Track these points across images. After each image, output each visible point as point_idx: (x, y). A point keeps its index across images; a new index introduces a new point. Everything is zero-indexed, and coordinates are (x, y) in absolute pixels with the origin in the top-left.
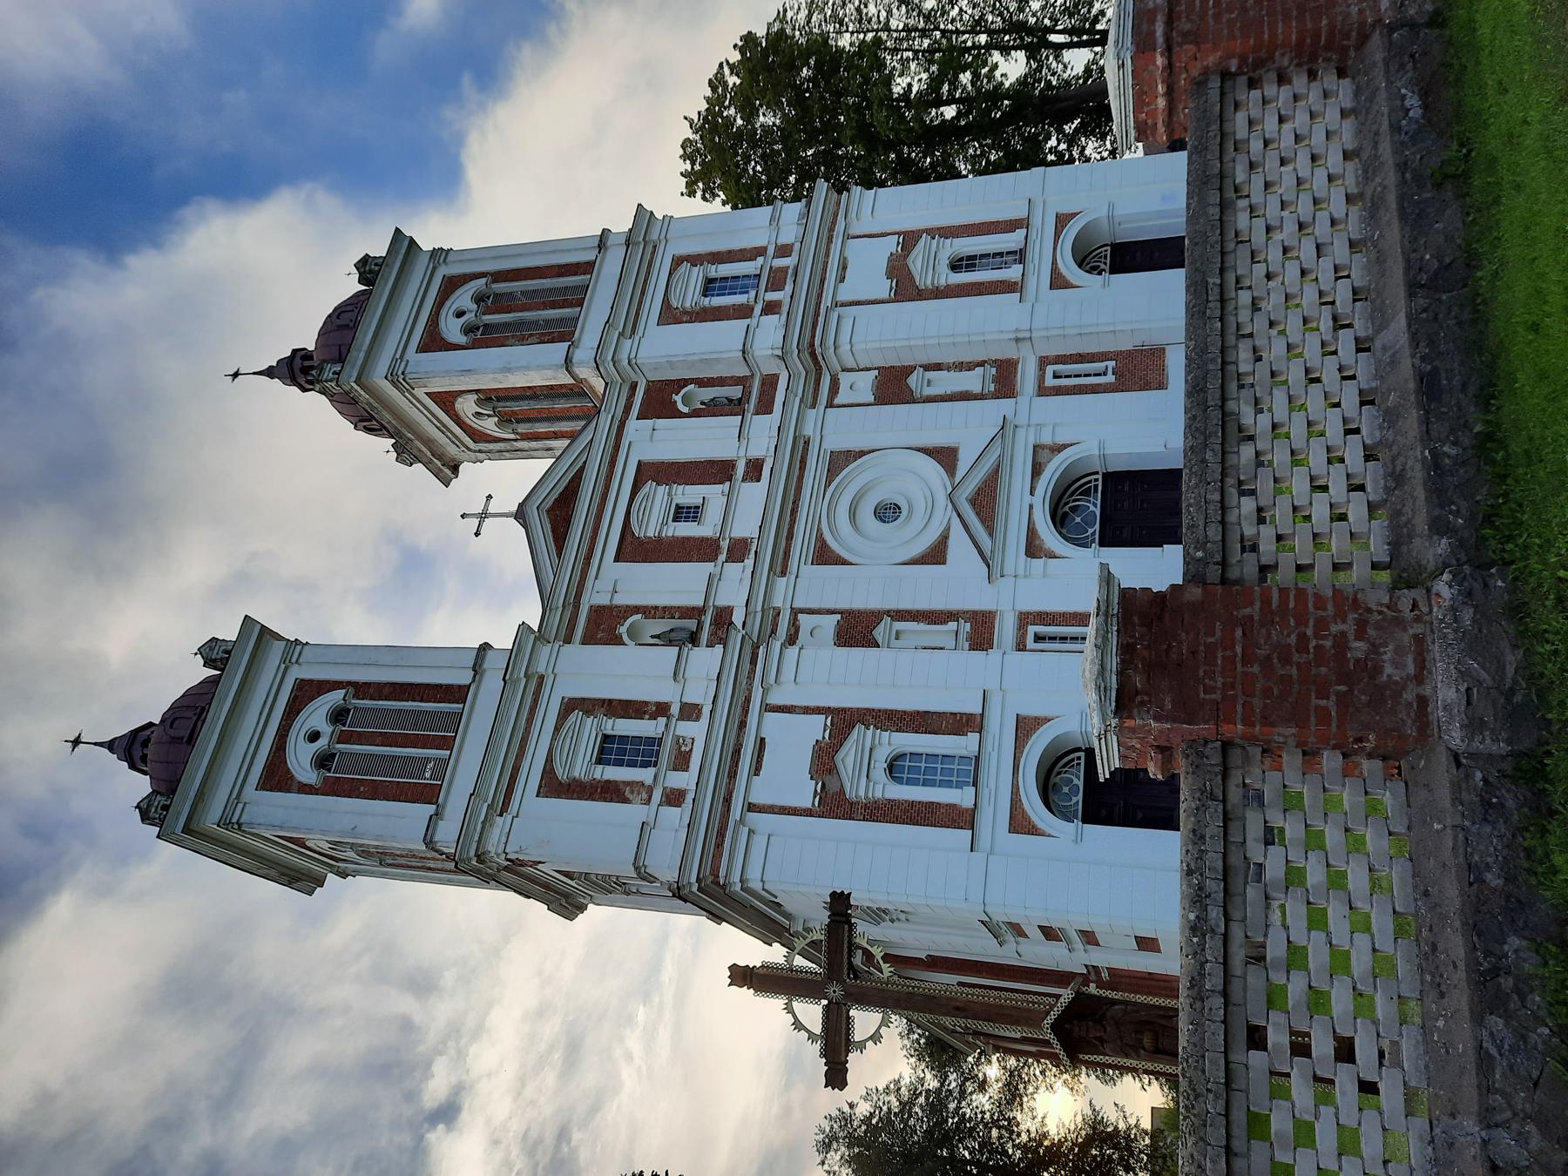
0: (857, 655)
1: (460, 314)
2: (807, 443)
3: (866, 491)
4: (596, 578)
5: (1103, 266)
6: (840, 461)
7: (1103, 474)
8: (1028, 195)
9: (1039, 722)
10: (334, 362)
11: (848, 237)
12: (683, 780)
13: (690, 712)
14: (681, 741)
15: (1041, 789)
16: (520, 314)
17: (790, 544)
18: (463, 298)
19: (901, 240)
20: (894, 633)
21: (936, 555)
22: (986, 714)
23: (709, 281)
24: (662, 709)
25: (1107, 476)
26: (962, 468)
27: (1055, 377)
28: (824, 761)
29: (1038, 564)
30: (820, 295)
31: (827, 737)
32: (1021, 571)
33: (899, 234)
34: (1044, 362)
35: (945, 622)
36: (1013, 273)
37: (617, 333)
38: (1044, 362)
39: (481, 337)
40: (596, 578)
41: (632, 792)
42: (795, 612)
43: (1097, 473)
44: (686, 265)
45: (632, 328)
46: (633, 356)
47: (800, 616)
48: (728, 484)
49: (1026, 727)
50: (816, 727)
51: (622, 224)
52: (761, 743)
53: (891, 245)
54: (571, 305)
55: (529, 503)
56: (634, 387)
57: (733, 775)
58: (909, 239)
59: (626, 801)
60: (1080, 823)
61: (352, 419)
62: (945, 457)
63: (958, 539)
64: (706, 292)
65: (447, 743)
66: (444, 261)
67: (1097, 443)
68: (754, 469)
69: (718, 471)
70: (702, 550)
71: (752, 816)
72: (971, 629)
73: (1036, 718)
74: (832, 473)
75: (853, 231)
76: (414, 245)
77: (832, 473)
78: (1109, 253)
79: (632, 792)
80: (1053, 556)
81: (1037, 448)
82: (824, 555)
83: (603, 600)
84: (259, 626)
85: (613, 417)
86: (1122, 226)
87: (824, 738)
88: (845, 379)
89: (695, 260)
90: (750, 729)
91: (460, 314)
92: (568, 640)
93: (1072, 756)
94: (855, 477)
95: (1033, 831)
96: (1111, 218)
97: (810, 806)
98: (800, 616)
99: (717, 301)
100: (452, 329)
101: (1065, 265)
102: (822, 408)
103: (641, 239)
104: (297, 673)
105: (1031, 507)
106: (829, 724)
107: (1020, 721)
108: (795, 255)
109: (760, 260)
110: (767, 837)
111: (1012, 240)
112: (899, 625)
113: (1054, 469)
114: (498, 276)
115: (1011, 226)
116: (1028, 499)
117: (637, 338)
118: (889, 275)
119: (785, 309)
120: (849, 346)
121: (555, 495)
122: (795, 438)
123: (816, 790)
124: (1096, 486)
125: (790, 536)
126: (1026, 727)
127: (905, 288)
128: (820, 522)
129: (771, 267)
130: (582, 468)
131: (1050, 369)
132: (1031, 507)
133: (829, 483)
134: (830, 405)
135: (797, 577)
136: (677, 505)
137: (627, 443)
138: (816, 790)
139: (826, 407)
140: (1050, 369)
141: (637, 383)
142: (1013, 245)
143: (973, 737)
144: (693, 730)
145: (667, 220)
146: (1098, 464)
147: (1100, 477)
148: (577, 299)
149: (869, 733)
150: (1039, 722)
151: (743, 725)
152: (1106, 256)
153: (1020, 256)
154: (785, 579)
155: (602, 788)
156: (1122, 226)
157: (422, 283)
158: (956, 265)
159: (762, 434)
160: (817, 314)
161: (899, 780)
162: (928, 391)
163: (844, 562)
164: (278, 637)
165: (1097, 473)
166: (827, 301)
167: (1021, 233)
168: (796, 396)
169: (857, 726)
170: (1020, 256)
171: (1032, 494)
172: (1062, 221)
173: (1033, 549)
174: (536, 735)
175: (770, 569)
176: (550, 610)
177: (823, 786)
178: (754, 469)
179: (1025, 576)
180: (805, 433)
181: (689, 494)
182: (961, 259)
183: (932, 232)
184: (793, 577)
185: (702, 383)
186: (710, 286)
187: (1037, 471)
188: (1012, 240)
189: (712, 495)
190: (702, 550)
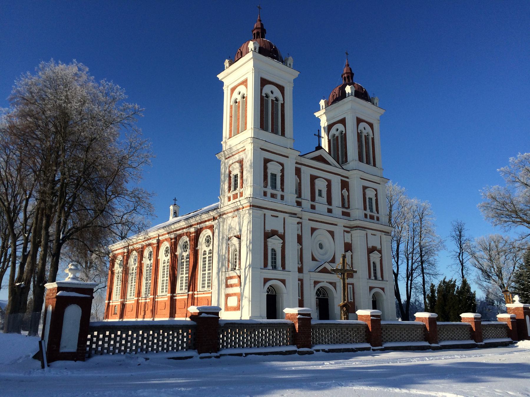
0: (354, 247)
1: (272, 92)
5: (270, 292)
9: (285, 284)
16: (364, 145)
21: (314, 259)
23: (275, 175)
28: (274, 233)
33: (284, 233)
34: (353, 284)
35: (300, 261)
36: (373, 278)
38: (353, 284)
44: (281, 168)
47: (300, 224)
53: (281, 231)
64: (369, 198)
69: (329, 202)
70: (313, 199)
78: (273, 294)
80: (314, 287)
91: (272, 92)
98: (300, 224)
100: (268, 89)
109: (376, 212)
116: (325, 281)
118: (272, 231)
124: (325, 297)
127: (371, 250)
131: (351, 286)
140: (351, 286)
147: (327, 298)
150: (285, 284)
152: (272, 293)
153: (274, 267)
158: (374, 263)
167: (381, 279)
170: (376, 278)
171: (326, 282)
181: (324, 194)
182: (375, 264)
183: (381, 257)
185: (348, 196)
187: (331, 283)
189: (324, 200)
190: (313, 199)
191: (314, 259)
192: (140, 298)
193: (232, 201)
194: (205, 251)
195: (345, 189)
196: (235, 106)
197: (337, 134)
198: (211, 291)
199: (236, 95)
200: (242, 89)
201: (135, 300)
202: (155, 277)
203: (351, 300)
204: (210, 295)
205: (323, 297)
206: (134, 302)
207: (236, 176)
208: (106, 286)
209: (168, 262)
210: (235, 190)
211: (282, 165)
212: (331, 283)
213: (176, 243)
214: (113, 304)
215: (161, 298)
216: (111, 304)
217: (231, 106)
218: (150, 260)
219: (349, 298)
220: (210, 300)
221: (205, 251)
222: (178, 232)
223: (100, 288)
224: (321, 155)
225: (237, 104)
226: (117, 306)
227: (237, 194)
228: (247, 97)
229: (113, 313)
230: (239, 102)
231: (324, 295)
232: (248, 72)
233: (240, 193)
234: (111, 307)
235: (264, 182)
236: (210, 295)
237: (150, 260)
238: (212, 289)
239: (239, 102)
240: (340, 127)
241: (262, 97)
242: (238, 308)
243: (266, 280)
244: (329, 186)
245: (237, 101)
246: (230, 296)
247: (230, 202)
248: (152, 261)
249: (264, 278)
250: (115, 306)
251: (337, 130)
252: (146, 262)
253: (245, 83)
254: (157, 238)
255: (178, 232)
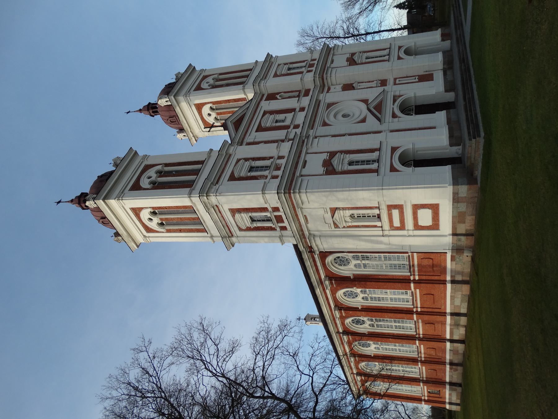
1: (149, 178)
2: (320, 101)
4: (249, 136)
6: (329, 105)
7: (415, 106)
8: (380, 140)
10: (96, 194)
11: (307, 153)
12: (279, 173)
14: (278, 165)
17: (314, 123)
18: (152, 173)
19: (325, 169)
21: (364, 121)
22: (380, 158)
25: (416, 106)
27: (399, 81)
29: (396, 119)
30: (326, 63)
31: (350, 56)
32: (391, 121)
33: (328, 152)
36: (374, 166)
37: (210, 183)
39: (157, 186)
40: (249, 136)
43: (413, 106)
45: (265, 77)
48: (293, 113)
51: (262, 59)
55: (229, 119)
56: (263, 95)
57: (296, 168)
58: (332, 154)
61: (164, 118)
62: (365, 101)
66: (147, 159)
67: (413, 93)
68: (302, 109)
73: (397, 147)
74: (328, 108)
75: (309, 151)
76: (136, 154)
77: (328, 108)
78: (413, 163)
81: (394, 97)
82: (325, 124)
85: (257, 100)
86: (419, 49)
87: (327, 158)
89: (246, 160)
90: (298, 170)
92: (241, 145)
93: (409, 162)
94: (334, 109)
95: (402, 59)
96: (413, 148)
101: (397, 165)
102: (325, 93)
103: (268, 60)
105: (393, 109)
108: (286, 159)
110: (307, 180)
111: (375, 155)
113: (399, 101)
114: (167, 165)
115: (372, 151)
116: (392, 106)
117: (266, 80)
119: (282, 169)
120: (335, 76)
121: (236, 119)
122: (316, 100)
125: (314, 121)
129: (309, 63)
132: (393, 109)
133: (327, 110)
135: (317, 129)
136: (276, 120)
137: (261, 106)
139: (326, 93)
140: (397, 80)
141: (264, 94)
142: (374, 157)
144: (283, 162)
145: (276, 57)
146: (412, 151)
147: (414, 107)
148: (196, 172)
149: (342, 155)
151: (299, 157)
153: (378, 161)
154: (313, 130)
156: (419, 49)
157: (197, 76)
159: (305, 101)
160: (324, 70)
162: (359, 87)
165: (413, 106)
166: (298, 174)
167: (377, 153)
168: (317, 90)
169: (338, 153)
172: (394, 149)
175: (308, 127)
176: (234, 143)
177: (326, 169)
178: (302, 109)
179: (392, 122)
180: (320, 99)
183: (341, 152)
184: (315, 129)
186: (251, 169)
187: (394, 101)
188: (375, 155)
189: (290, 116)
191: (364, 121)
192: (419, 359)
193: (286, 224)
194: (363, 298)
195: (276, 96)
196: (168, 224)
197: (214, 115)
198: (410, 254)
199: (154, 225)
200: (145, 215)
201: (422, 366)
202: (391, 338)
203: (416, 78)
204: (415, 255)
205: (413, 111)
206: (424, 368)
207: (253, 220)
208: (402, 405)
209: (365, 292)
210: (272, 221)
211: (238, 160)
212: (394, 101)
213: (347, 308)
214: (426, 395)
215: (419, 330)
216: (426, 398)
217: (169, 231)
218: (363, 322)
219: (414, 81)
220: (422, 256)
221: (363, 298)
222: (333, 306)
223: (405, 412)
224: (281, 215)
225: (164, 222)
226: (429, 390)
227: (275, 216)
228: (153, 208)
229: (438, 396)
230: (161, 219)
231: (410, 110)
232: (123, 207)
233: (274, 211)
234: (431, 398)
235: (259, 179)
236: (415, 255)
237: (363, 322)
238: (407, 253)
239: (161, 219)
240: (206, 110)
241: (153, 188)
242: (435, 208)
243: (393, 169)
244: (272, 112)
245: (160, 222)
246: (417, 223)
247: (288, 227)
248: (365, 319)
249: (390, 172)
250: (429, 392)
251: (209, 115)
252: (372, 348)
253: (137, 211)
254: (341, 334)
255: (333, 306)
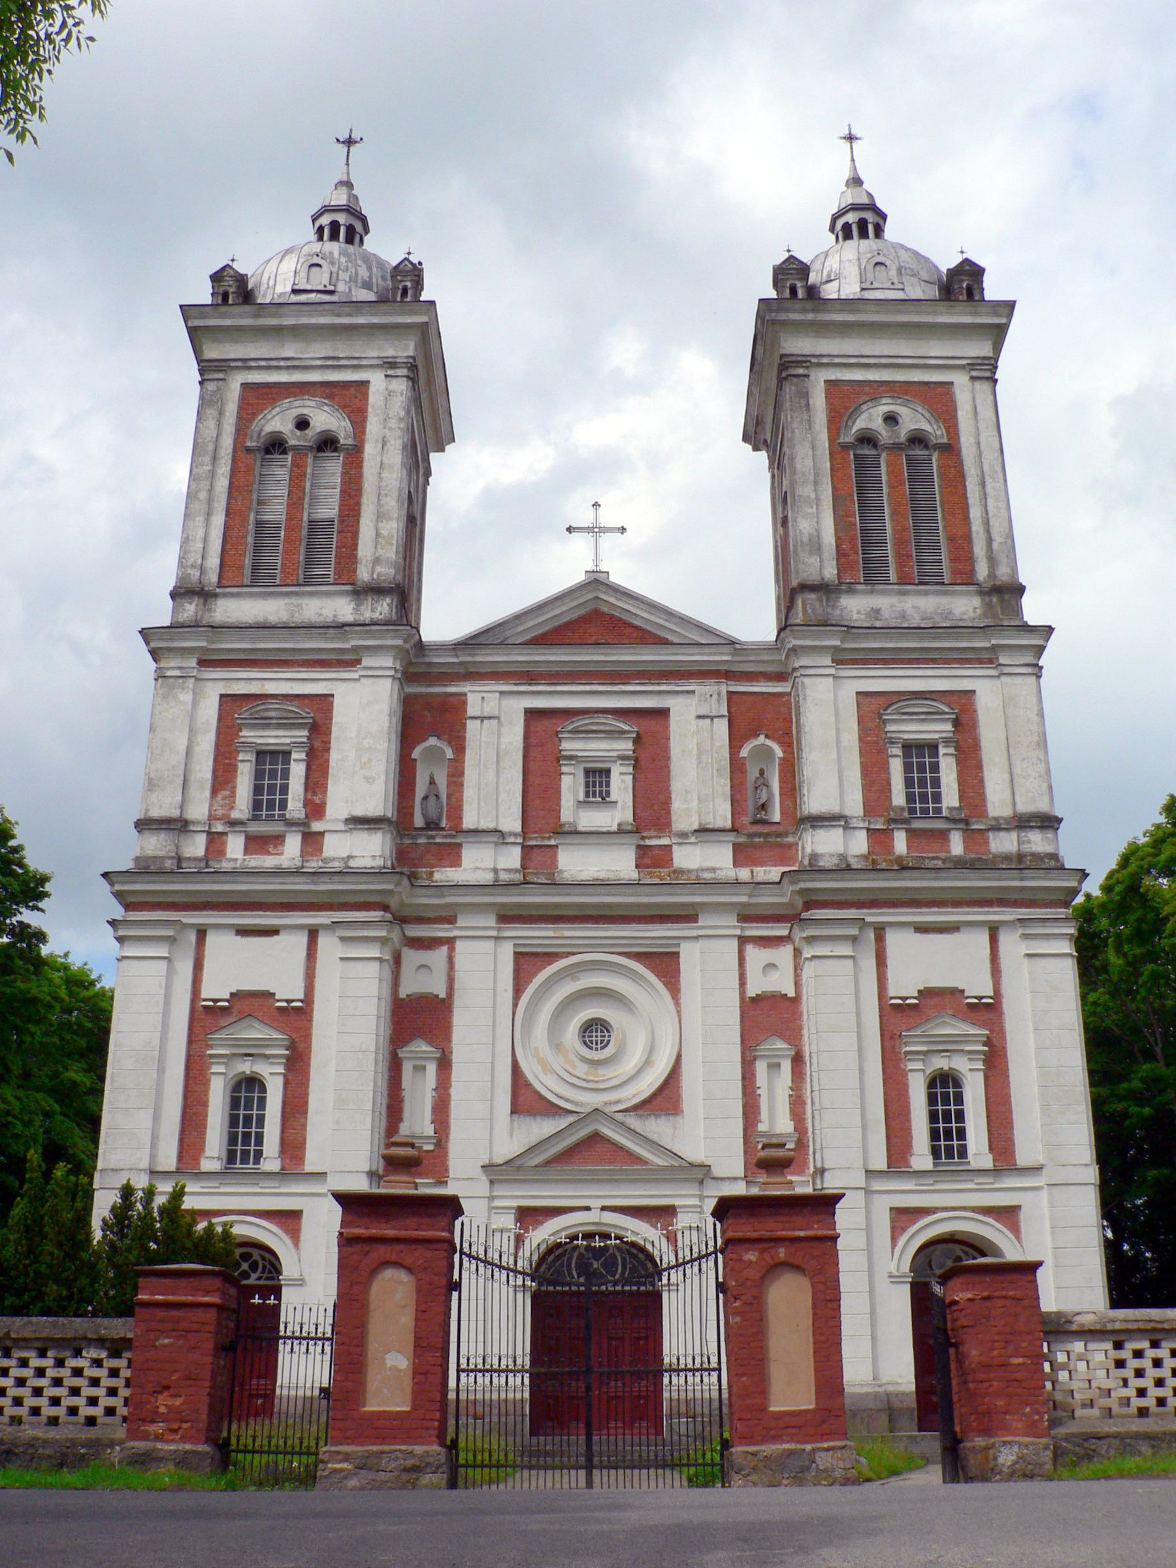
3: (621, 1001)
9: (1015, 1229)
13: (312, 840)
15: (941, 1237)
20: (776, 1060)
24: (316, 809)
26: (632, 1121)
32: (498, 1203)
41: (224, 798)
42: (450, 942)
46: (803, 672)
49: (1008, 1215)
50: (978, 986)
52: (272, 932)
54: (901, 566)
55: (602, 588)
56: (781, 677)
59: (214, 792)
60: (910, 1280)
63: (545, 1127)
65: (904, 580)
71: (192, 937)
72: (426, 1151)
79: (224, 798)
83: (474, 706)
84: (1004, 320)
88: (783, 955)
95: (896, 1231)
97: (203, 996)
99: (896, 767)
104: (960, 380)
105: (588, 1209)
106: (908, 1001)
107: (296, 1215)
112: (786, 1066)
116: (596, 1204)
123: (293, 1001)
126: (1008, 1215)
128: (574, 954)
130: (666, 642)
132: (588, 1209)
133: (638, 956)
134: (743, 941)
138: (293, 1001)
143: (987, 1162)
155: (230, 764)
161: (932, 1084)
163: (518, 991)
164: (998, 346)
171: (604, 1209)
173: (903, 1217)
174: (334, 675)
181: (621, 784)
